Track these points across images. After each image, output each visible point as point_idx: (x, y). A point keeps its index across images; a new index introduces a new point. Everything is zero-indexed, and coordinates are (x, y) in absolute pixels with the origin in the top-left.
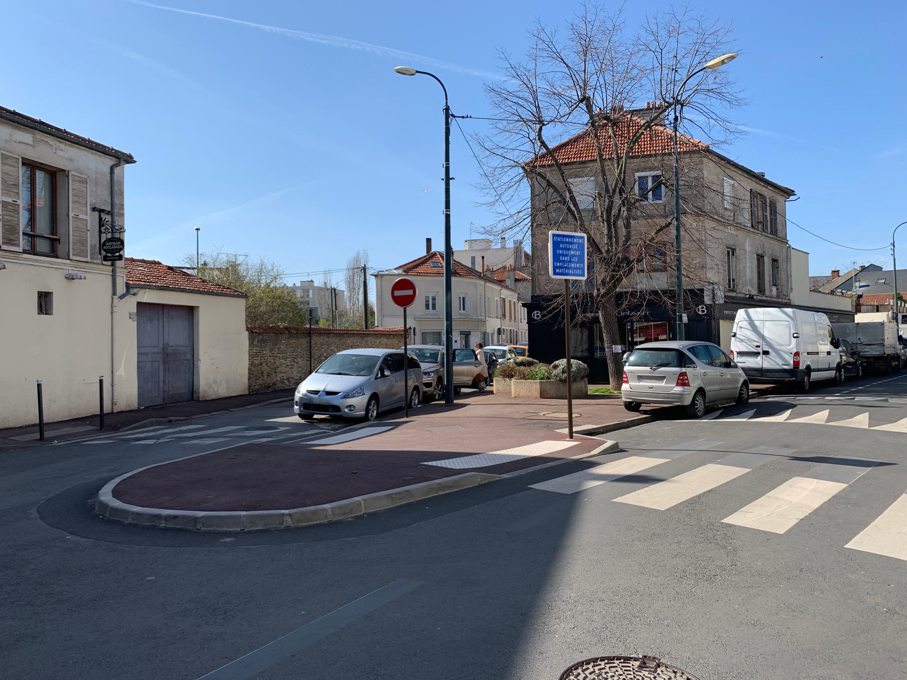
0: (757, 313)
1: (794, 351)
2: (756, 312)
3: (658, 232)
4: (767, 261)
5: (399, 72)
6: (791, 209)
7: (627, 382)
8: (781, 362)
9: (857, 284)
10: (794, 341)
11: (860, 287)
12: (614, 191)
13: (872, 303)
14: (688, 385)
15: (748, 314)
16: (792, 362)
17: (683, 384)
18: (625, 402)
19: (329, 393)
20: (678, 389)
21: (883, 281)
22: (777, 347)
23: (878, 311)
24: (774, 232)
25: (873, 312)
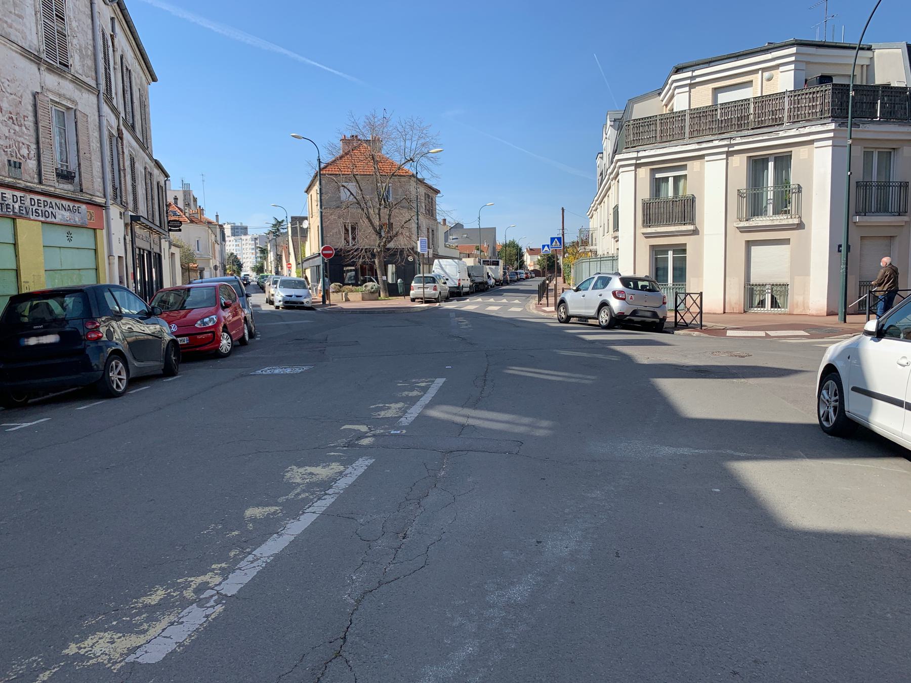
0: (443, 262)
1: (459, 279)
2: (443, 261)
3: (405, 223)
4: (430, 230)
5: (293, 136)
6: (438, 199)
7: (413, 290)
8: (453, 284)
9: (451, 237)
10: (458, 274)
11: (453, 239)
12: (381, 199)
13: (466, 252)
14: (437, 290)
15: (439, 262)
16: (457, 283)
17: (435, 290)
18: (411, 298)
19: (297, 296)
20: (434, 292)
21: (466, 236)
22: (452, 277)
23: (469, 257)
24: (432, 215)
25: (466, 258)
